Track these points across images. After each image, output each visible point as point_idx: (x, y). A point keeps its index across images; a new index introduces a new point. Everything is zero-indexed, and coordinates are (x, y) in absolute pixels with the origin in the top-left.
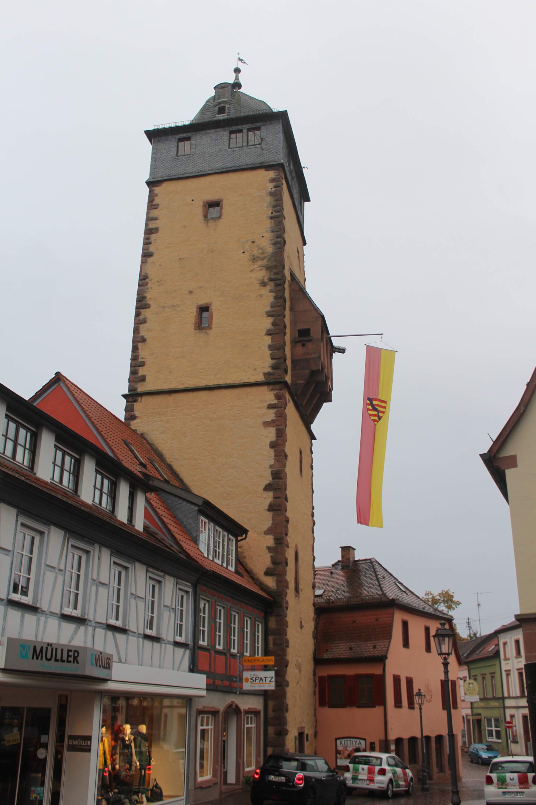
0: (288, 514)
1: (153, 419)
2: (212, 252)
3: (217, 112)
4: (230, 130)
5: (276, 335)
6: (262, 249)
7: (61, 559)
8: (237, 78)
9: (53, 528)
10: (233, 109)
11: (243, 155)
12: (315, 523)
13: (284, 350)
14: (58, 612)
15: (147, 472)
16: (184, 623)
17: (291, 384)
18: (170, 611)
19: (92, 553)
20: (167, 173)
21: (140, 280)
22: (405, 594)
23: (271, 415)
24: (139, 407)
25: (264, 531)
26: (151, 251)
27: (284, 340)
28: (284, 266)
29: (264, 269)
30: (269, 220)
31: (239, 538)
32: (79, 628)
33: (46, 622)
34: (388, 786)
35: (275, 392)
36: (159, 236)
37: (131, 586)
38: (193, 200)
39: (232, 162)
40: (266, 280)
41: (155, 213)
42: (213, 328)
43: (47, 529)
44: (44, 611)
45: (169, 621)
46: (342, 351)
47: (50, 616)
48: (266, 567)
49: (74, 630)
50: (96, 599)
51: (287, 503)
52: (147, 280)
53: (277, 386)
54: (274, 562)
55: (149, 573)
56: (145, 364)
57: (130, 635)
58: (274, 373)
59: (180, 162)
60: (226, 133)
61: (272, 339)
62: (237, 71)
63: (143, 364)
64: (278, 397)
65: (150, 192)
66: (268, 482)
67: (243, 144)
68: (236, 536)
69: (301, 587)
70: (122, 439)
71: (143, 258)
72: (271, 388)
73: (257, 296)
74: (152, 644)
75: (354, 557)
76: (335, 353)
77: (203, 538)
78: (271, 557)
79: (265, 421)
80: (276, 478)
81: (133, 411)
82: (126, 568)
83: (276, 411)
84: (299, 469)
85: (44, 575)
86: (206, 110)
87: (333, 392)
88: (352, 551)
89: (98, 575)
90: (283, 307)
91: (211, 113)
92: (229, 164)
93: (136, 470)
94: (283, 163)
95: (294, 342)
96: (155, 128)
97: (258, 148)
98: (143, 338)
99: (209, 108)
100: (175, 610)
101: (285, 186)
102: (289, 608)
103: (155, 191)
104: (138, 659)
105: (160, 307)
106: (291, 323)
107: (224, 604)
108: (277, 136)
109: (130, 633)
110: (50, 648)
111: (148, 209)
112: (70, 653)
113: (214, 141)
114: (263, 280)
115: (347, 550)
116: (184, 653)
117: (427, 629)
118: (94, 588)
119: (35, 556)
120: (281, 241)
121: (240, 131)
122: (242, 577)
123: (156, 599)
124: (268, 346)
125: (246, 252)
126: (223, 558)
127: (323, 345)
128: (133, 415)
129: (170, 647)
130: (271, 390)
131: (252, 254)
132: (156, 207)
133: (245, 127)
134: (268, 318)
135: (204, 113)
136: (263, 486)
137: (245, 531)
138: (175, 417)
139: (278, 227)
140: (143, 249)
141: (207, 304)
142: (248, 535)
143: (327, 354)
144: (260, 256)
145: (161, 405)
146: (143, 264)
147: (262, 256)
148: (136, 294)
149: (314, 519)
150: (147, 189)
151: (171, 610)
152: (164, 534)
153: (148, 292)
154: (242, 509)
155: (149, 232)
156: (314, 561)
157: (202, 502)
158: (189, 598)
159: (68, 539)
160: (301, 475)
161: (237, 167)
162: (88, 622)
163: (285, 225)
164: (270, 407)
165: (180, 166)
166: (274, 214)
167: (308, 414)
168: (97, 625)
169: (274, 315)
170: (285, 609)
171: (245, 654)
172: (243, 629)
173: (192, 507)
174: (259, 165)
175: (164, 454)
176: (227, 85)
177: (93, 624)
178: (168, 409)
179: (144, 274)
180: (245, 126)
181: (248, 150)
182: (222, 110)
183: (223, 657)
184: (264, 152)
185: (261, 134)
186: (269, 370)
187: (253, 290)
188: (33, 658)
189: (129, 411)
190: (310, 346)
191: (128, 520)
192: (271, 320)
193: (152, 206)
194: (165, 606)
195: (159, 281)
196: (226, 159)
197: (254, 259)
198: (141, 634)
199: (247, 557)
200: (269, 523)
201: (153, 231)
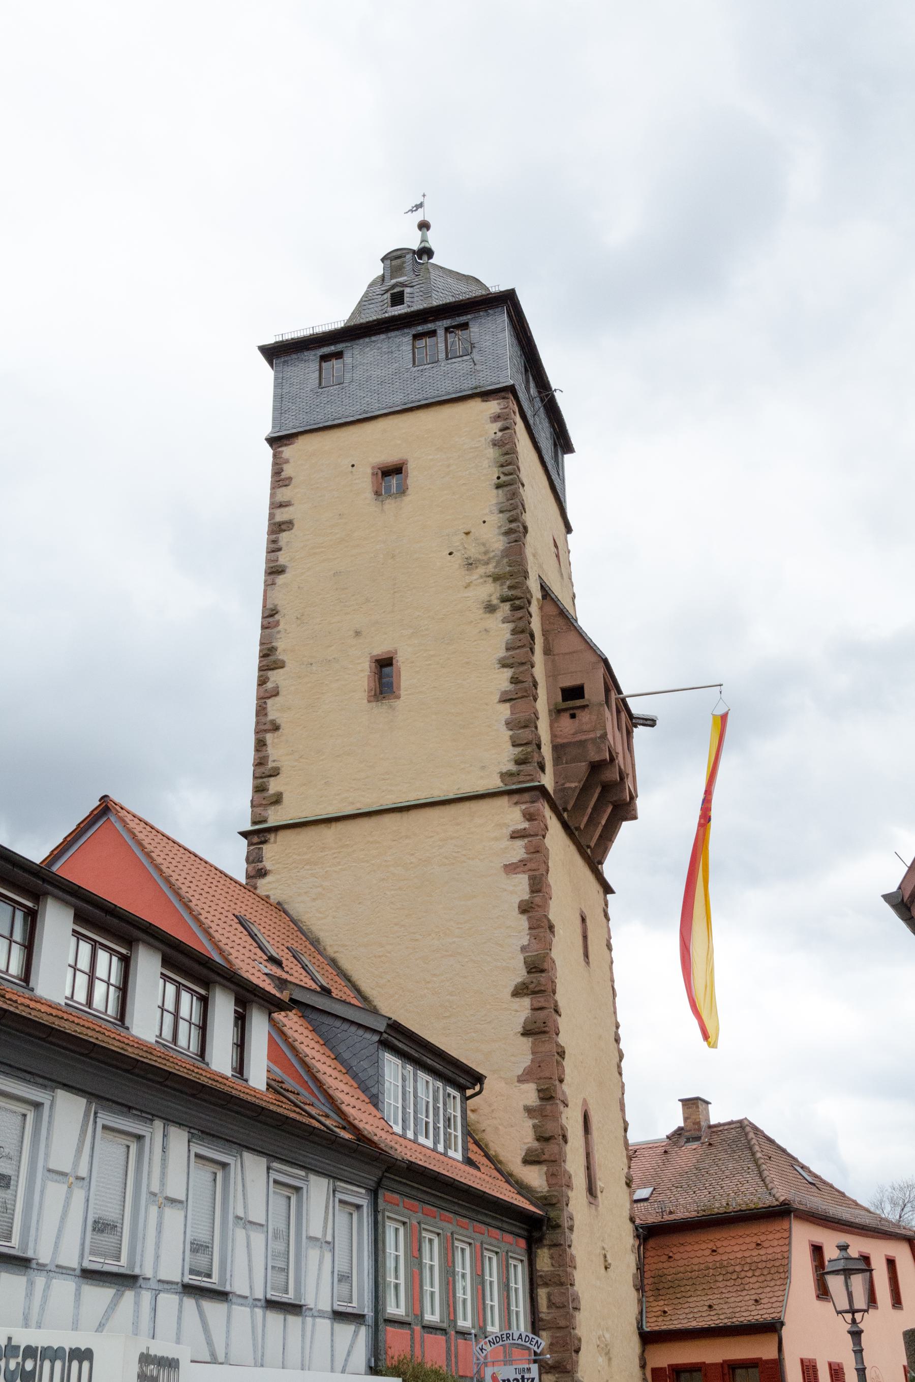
0: (562, 1039)
1: (298, 874)
2: (393, 557)
3: (389, 302)
4: (414, 332)
5: (519, 700)
6: (484, 545)
7: (81, 1156)
8: (424, 240)
9: (61, 1094)
10: (416, 294)
11: (440, 377)
12: (623, 1055)
13: (536, 728)
14: (74, 1264)
15: (284, 973)
17: (555, 791)
18: (321, 1247)
20: (304, 420)
21: (263, 618)
22: (814, 1189)
23: (518, 851)
24: (271, 852)
25: (518, 1076)
26: (282, 563)
27: (534, 707)
29: (490, 580)
30: (495, 491)
31: (469, 1092)
32: (122, 1295)
33: (47, 1287)
35: (524, 807)
36: (295, 536)
37: (235, 1201)
38: (353, 466)
39: (420, 391)
40: (495, 601)
41: (284, 494)
42: (402, 696)
43: (47, 1096)
44: (44, 1265)
45: (320, 1269)
46: (650, 722)
47: (57, 1275)
48: (526, 1147)
49: (112, 1301)
51: (558, 1017)
52: (277, 617)
53: (526, 796)
54: (543, 1138)
55: (274, 1172)
56: (280, 772)
57: (235, 1304)
58: (519, 771)
59: (325, 399)
60: (408, 339)
62: (424, 226)
63: (275, 773)
64: (530, 817)
65: (275, 456)
66: (520, 980)
68: (462, 1088)
69: (600, 1184)
70: (234, 915)
71: (268, 577)
72: (515, 801)
73: (480, 632)
74: (285, 1320)
75: (708, 1119)
76: (636, 727)
77: (392, 1099)
78: (534, 1126)
79: (508, 863)
80: (534, 970)
83: (526, 842)
84: (581, 951)
86: (370, 300)
88: (704, 1105)
89: (163, 1183)
90: (529, 649)
91: (378, 305)
93: (259, 971)
95: (556, 712)
96: (277, 340)
98: (275, 724)
99: (374, 297)
100: (332, 1245)
101: (520, 427)
102: (575, 1229)
103: (284, 454)
104: (255, 1352)
106: (547, 676)
107: (438, 1228)
108: (501, 336)
109: (234, 1300)
111: (273, 488)
113: (386, 356)
116: (356, 1333)
118: (154, 1210)
120: (518, 527)
121: (433, 333)
124: (505, 721)
125: (455, 553)
126: (436, 1135)
128: (262, 869)
129: (325, 1324)
130: (516, 803)
131: (466, 556)
132: (287, 482)
133: (440, 326)
134: (502, 670)
135: (365, 308)
136: (511, 988)
137: (478, 1079)
138: (340, 867)
139: (510, 502)
140: (268, 561)
141: (389, 652)
142: (485, 1086)
143: (619, 728)
144: (480, 557)
145: (312, 847)
146: (269, 588)
147: (485, 558)
148: (258, 643)
149: (621, 1046)
150: (268, 451)
151: (324, 1245)
153: (280, 638)
154: (474, 1035)
155: (278, 528)
156: (626, 1130)
157: (385, 1025)
158: (363, 1219)
159: (96, 1113)
160: (588, 963)
161: (431, 398)
162: (141, 1281)
163: (524, 498)
165: (326, 405)
166: (503, 478)
167: (592, 844)
168: (161, 1287)
169: (512, 664)
170: (567, 1230)
171: (489, 1328)
172: (482, 1276)
173: (368, 1035)
174: (470, 392)
175: (321, 939)
176: (404, 251)
177: (153, 1284)
178: (326, 853)
179: (271, 606)
180: (439, 323)
181: (448, 366)
182: (398, 299)
183: (441, 1338)
186: (512, 767)
187: (472, 622)
189: (253, 862)
190: (584, 717)
191: (234, 1069)
192: (508, 673)
193: (279, 481)
194: (310, 1238)
195: (299, 616)
196: (408, 386)
197: (470, 565)
198: (259, 1300)
199: (488, 1129)
201: (283, 527)
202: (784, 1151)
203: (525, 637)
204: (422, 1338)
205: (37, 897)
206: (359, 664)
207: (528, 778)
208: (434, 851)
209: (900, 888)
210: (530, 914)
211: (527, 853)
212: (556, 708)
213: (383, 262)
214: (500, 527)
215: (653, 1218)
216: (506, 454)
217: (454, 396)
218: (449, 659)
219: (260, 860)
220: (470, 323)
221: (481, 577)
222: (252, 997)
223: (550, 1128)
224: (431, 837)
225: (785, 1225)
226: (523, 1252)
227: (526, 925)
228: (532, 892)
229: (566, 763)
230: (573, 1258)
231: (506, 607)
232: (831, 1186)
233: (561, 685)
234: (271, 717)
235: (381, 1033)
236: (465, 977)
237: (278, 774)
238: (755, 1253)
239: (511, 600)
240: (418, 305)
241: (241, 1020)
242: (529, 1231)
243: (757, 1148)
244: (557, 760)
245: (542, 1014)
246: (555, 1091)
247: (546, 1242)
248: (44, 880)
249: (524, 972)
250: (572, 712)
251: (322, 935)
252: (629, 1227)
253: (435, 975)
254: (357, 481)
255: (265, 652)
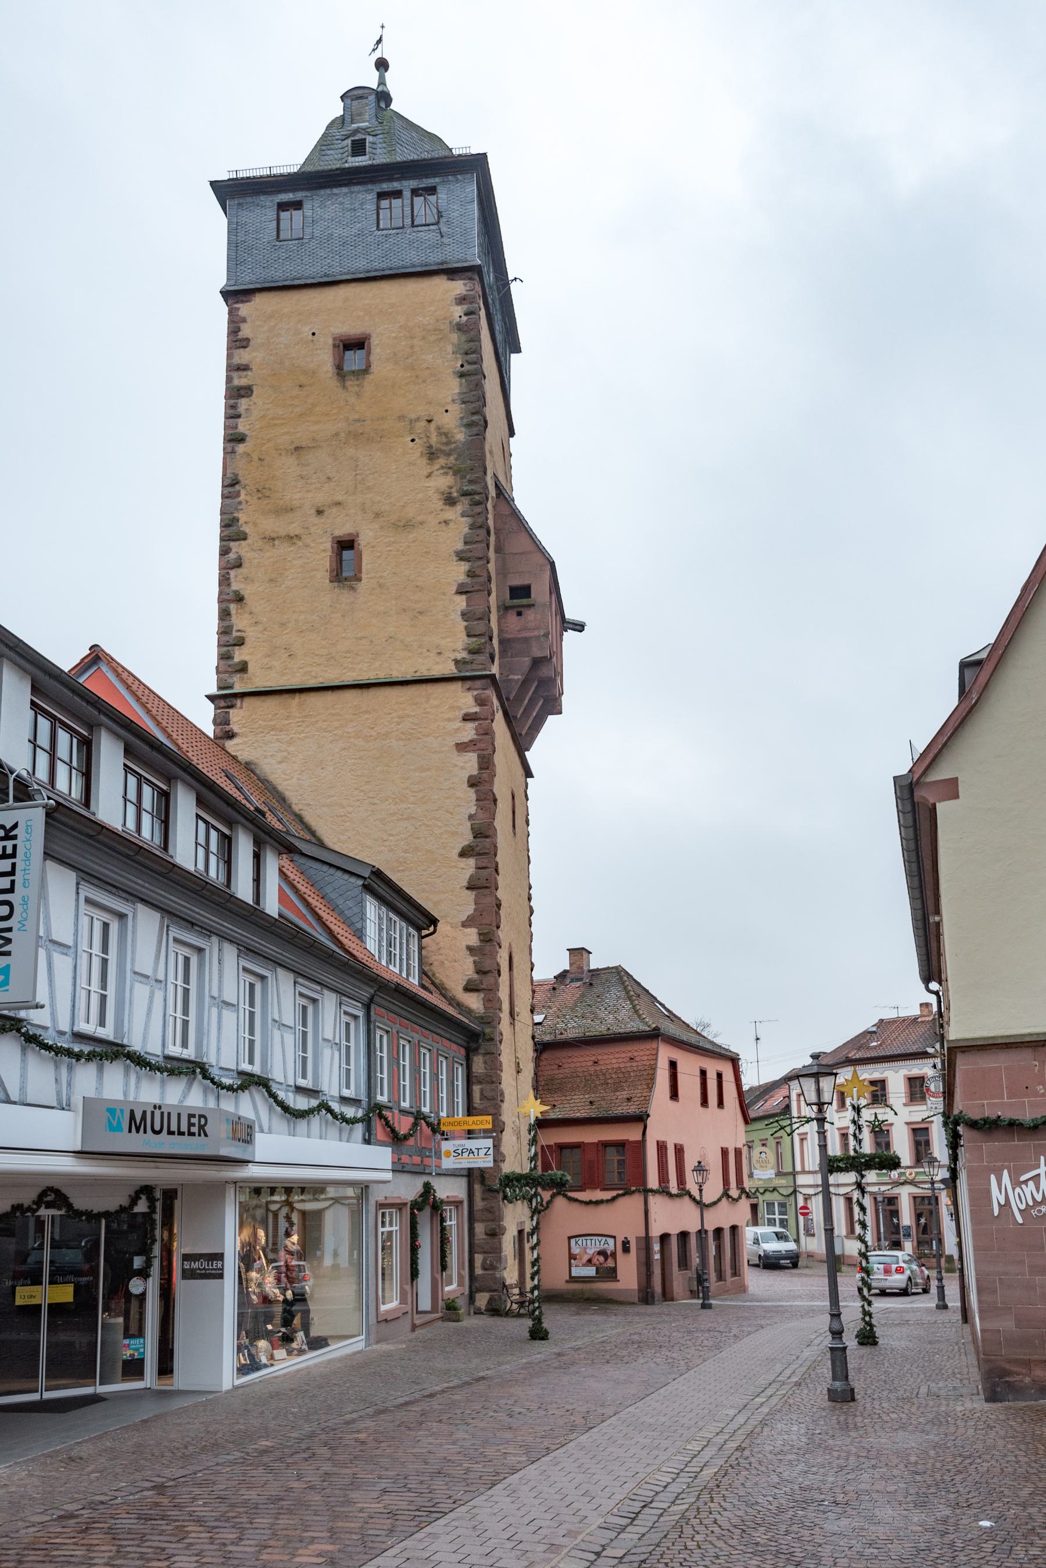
6: (446, 435)
8: (382, 82)
9: (140, 907)
10: (380, 145)
16: (352, 1067)
19: (207, 952)
24: (237, 717)
27: (488, 601)
28: (485, 468)
30: (458, 380)
31: (424, 932)
34: (907, 1285)
35: (475, 693)
40: (455, 494)
41: (243, 356)
42: (363, 578)
45: (331, 1064)
46: (579, 627)
48: (467, 978)
50: (219, 1029)
52: (237, 487)
53: (478, 683)
60: (372, 197)
61: (468, 601)
62: (382, 65)
63: (240, 642)
64: (481, 702)
65: (230, 313)
66: (466, 843)
67: (403, 221)
68: (419, 929)
71: (228, 445)
76: (566, 631)
77: (371, 930)
78: (475, 962)
81: (229, 724)
82: (263, 978)
84: (511, 823)
85: (131, 990)
87: (563, 698)
89: (220, 989)
91: (337, 152)
92: (378, 264)
94: (480, 266)
95: (504, 609)
97: (433, 231)
101: (483, 313)
105: (265, 538)
106: (497, 574)
110: (157, 1113)
112: (193, 1120)
114: (450, 493)
115: (578, 954)
117: (703, 1073)
118: (214, 1011)
119: (112, 956)
121: (398, 194)
122: (432, 993)
123: (310, 1030)
125: (417, 440)
127: (551, 616)
130: (469, 689)
134: (460, 562)
135: (323, 153)
137: (434, 921)
139: (473, 393)
140: (226, 427)
141: (350, 534)
144: (443, 448)
152: (310, 924)
153: (242, 509)
155: (236, 394)
159: (168, 927)
160: (515, 834)
164: (467, 718)
166: (467, 367)
173: (353, 880)
174: (435, 268)
176: (366, 91)
180: (405, 183)
182: (359, 148)
184: (445, 240)
185: (437, 202)
186: (463, 655)
188: (130, 1131)
189: (220, 724)
190: (530, 615)
193: (236, 341)
194: (325, 1040)
197: (432, 455)
198: (291, 1086)
199: (436, 963)
200: (470, 909)
201: (242, 392)
202: (647, 991)
203: (482, 532)
204: (399, 1118)
205: (91, 727)
206: (321, 543)
207: (481, 667)
208: (392, 726)
209: (910, 771)
210: (478, 788)
211: (477, 734)
212: (504, 605)
213: (343, 101)
214: (462, 418)
215: (547, 1038)
216: (471, 341)
217: (419, 269)
218: (409, 547)
219: (227, 722)
220: (438, 188)
221: (442, 468)
222: (267, 838)
223: (487, 965)
224: (390, 714)
225: (654, 1045)
226: (463, 1058)
227: (474, 797)
228: (481, 768)
229: (511, 657)
230: (501, 1063)
231: (466, 501)
232: (680, 1019)
233: (510, 584)
234: (235, 587)
235: (365, 878)
236: (418, 838)
237: (243, 644)
238: (629, 1064)
239: (470, 494)
240: (381, 158)
241: (258, 858)
242: (468, 1043)
243: (630, 988)
244: (503, 652)
245: (484, 873)
246: (493, 935)
247: (482, 1051)
248: (100, 711)
249: (471, 837)
250: (519, 610)
251: (288, 794)
252: (531, 1043)
253: (391, 835)
254: (318, 351)
255: (227, 522)
